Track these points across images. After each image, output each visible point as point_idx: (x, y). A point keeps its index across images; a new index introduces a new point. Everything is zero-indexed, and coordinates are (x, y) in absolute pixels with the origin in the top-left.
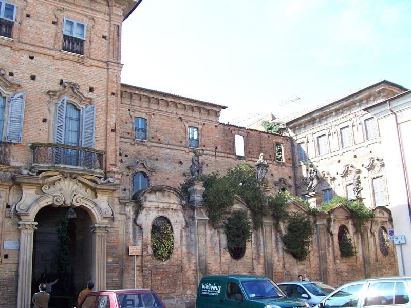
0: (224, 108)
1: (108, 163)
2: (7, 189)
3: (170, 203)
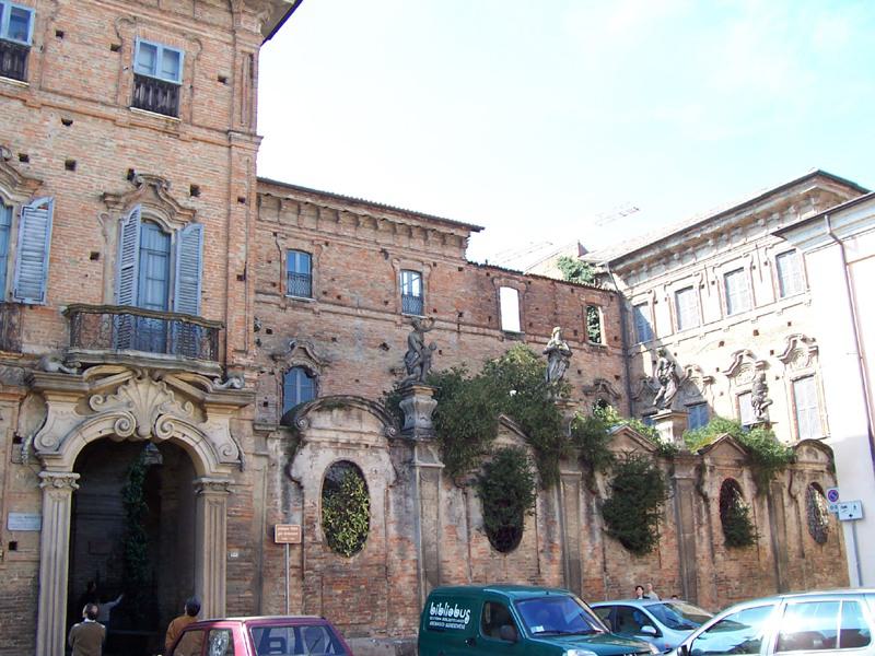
0: (477, 229)
1: (230, 348)
2: (14, 402)
3: (362, 433)
